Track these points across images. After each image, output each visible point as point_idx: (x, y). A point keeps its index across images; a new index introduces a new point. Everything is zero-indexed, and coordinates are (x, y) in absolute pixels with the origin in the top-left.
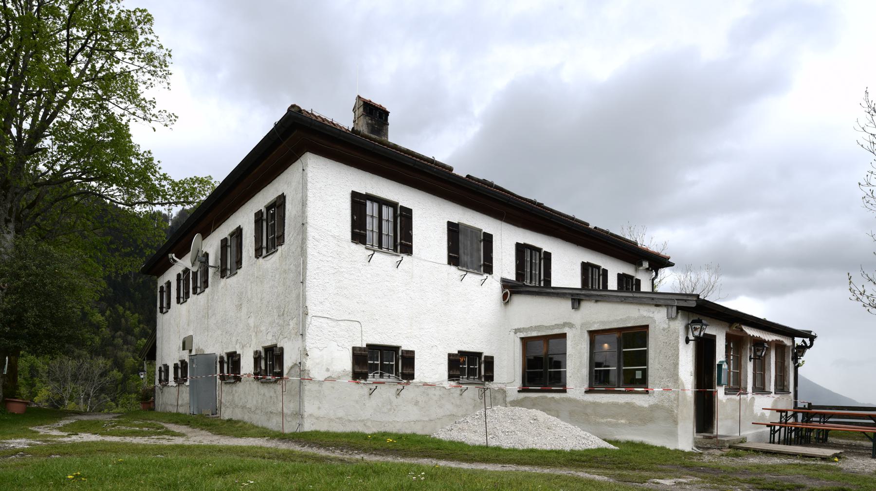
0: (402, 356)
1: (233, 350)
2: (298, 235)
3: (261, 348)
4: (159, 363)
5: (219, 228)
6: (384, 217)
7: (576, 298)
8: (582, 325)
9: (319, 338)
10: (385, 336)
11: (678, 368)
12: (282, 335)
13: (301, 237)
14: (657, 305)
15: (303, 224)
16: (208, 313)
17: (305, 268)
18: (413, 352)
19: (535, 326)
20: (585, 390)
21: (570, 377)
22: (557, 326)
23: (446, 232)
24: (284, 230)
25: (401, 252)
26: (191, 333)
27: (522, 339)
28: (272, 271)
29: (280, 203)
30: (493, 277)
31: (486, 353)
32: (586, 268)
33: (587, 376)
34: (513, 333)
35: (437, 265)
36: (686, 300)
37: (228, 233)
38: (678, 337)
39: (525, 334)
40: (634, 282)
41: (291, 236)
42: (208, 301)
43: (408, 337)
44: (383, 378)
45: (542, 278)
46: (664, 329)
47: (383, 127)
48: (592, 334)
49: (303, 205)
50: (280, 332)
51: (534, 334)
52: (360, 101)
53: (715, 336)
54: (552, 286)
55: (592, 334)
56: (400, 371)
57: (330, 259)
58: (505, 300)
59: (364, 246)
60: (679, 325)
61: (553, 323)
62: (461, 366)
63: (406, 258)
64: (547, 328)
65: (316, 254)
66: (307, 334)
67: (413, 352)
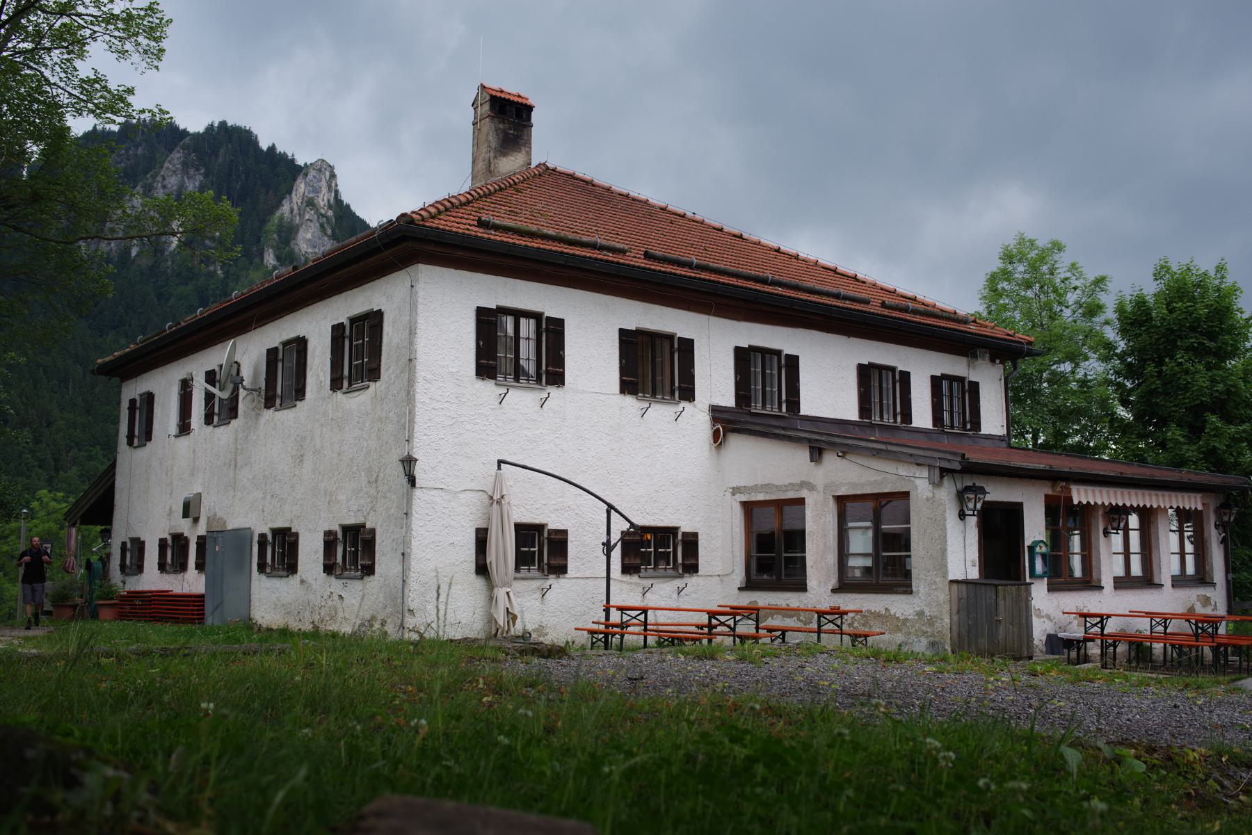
0: (548, 539)
1: (286, 525)
2: (402, 372)
4: (120, 534)
5: (263, 328)
6: (523, 333)
7: (815, 445)
8: (826, 487)
9: (430, 518)
10: (522, 509)
11: (946, 556)
12: (375, 511)
13: (407, 377)
14: (918, 464)
15: (410, 360)
16: (235, 459)
17: (412, 421)
18: (565, 532)
20: (831, 588)
21: (812, 567)
22: (792, 486)
23: (618, 345)
24: (380, 361)
25: (548, 383)
26: (199, 490)
28: (359, 415)
29: (371, 323)
30: (695, 406)
31: (686, 527)
32: (866, 373)
33: (834, 565)
34: (730, 494)
35: (602, 397)
36: (949, 461)
37: (281, 341)
38: (945, 511)
40: (967, 387)
41: (391, 371)
42: (236, 440)
43: (558, 510)
44: (520, 572)
45: (784, 397)
46: (928, 500)
47: (522, 131)
48: (841, 500)
49: (410, 334)
50: (370, 505)
51: (761, 497)
52: (484, 93)
53: (1021, 505)
54: (802, 412)
55: (841, 500)
56: (546, 561)
57: (446, 405)
58: (718, 439)
59: (493, 381)
60: (946, 494)
61: (787, 482)
63: (553, 390)
65: (427, 401)
67: (565, 532)
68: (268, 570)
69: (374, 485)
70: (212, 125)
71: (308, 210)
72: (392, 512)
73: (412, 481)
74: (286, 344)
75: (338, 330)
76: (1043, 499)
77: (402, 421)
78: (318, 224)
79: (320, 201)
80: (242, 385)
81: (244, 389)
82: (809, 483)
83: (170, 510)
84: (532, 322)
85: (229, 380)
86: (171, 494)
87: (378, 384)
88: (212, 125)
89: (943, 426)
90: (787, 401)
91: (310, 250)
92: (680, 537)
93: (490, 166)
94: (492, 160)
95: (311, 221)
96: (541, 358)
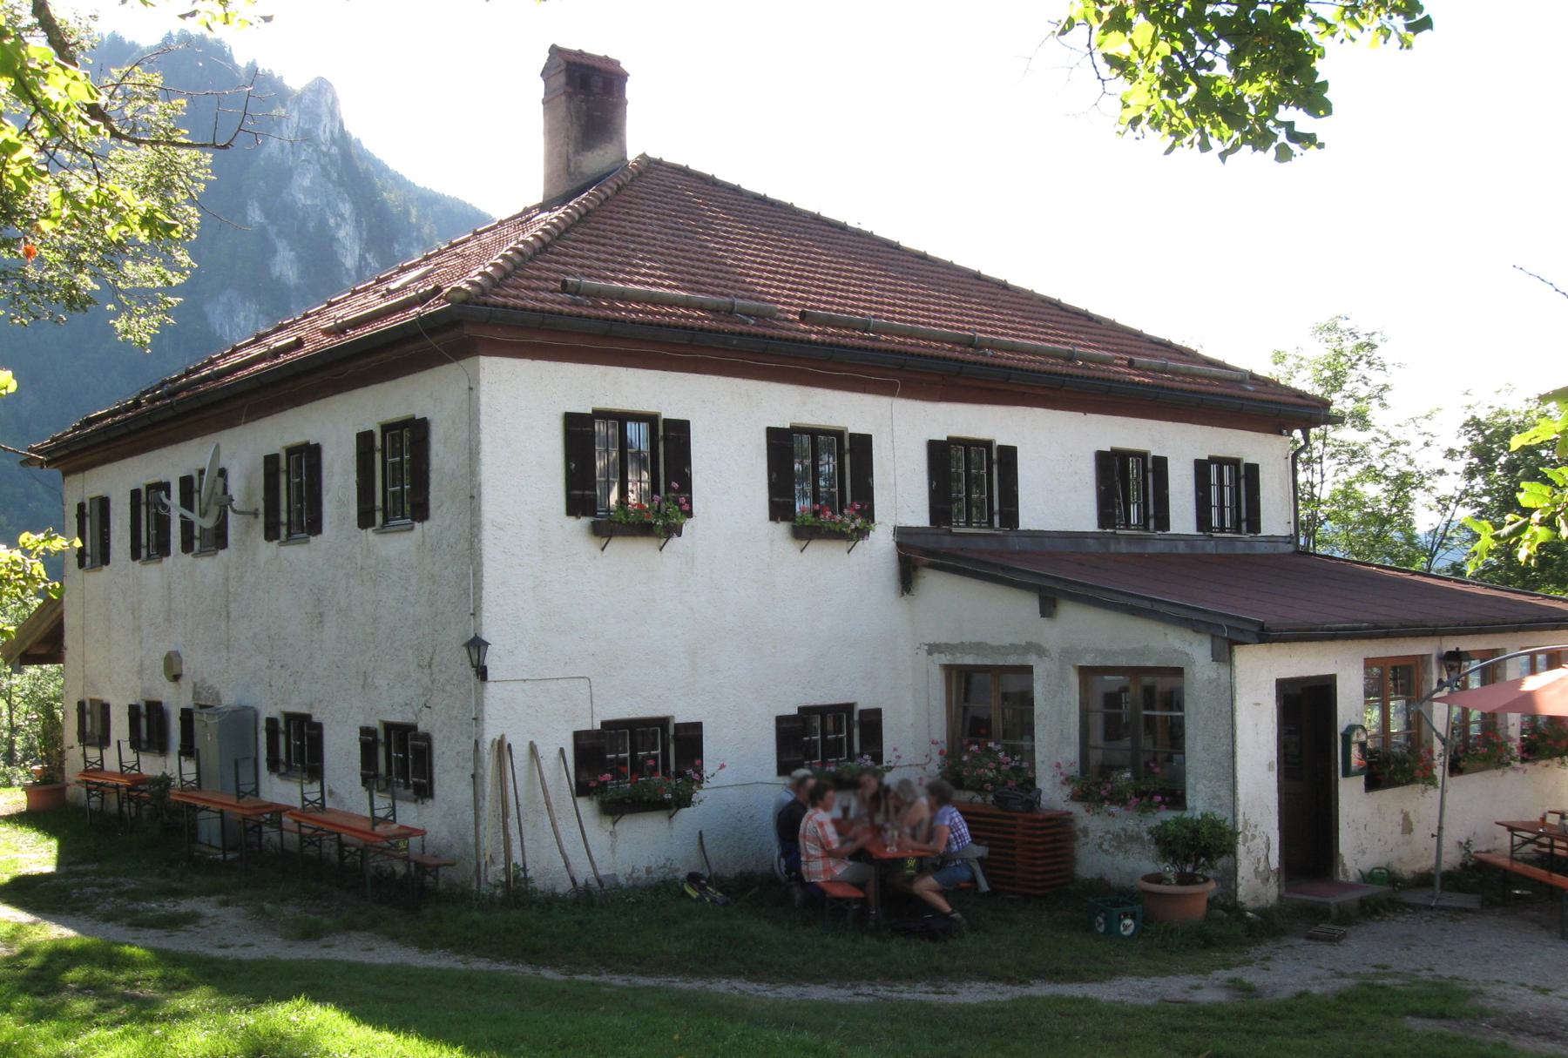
1: (304, 710)
3: (377, 723)
19: (970, 643)
21: (1043, 762)
22: (1014, 648)
27: (949, 669)
31: (864, 702)
34: (925, 653)
39: (949, 657)
42: (227, 580)
45: (996, 507)
49: (470, 459)
50: (423, 700)
56: (673, 768)
58: (907, 578)
61: (1007, 641)
62: (806, 739)
64: (995, 650)
66: (486, 717)
68: (283, 769)
69: (427, 671)
70: (170, 33)
71: (305, 147)
72: (455, 711)
73: (482, 673)
74: (291, 451)
75: (365, 439)
76: (1363, 661)
77: (464, 584)
78: (318, 166)
79: (321, 133)
80: (231, 507)
81: (235, 511)
82: (1040, 646)
83: (141, 665)
84: (644, 426)
85: (213, 501)
86: (141, 642)
87: (427, 524)
88: (170, 33)
89: (1210, 528)
90: (1001, 512)
91: (309, 202)
92: (856, 717)
93: (569, 166)
94: (571, 157)
95: (309, 162)
96: (659, 481)
